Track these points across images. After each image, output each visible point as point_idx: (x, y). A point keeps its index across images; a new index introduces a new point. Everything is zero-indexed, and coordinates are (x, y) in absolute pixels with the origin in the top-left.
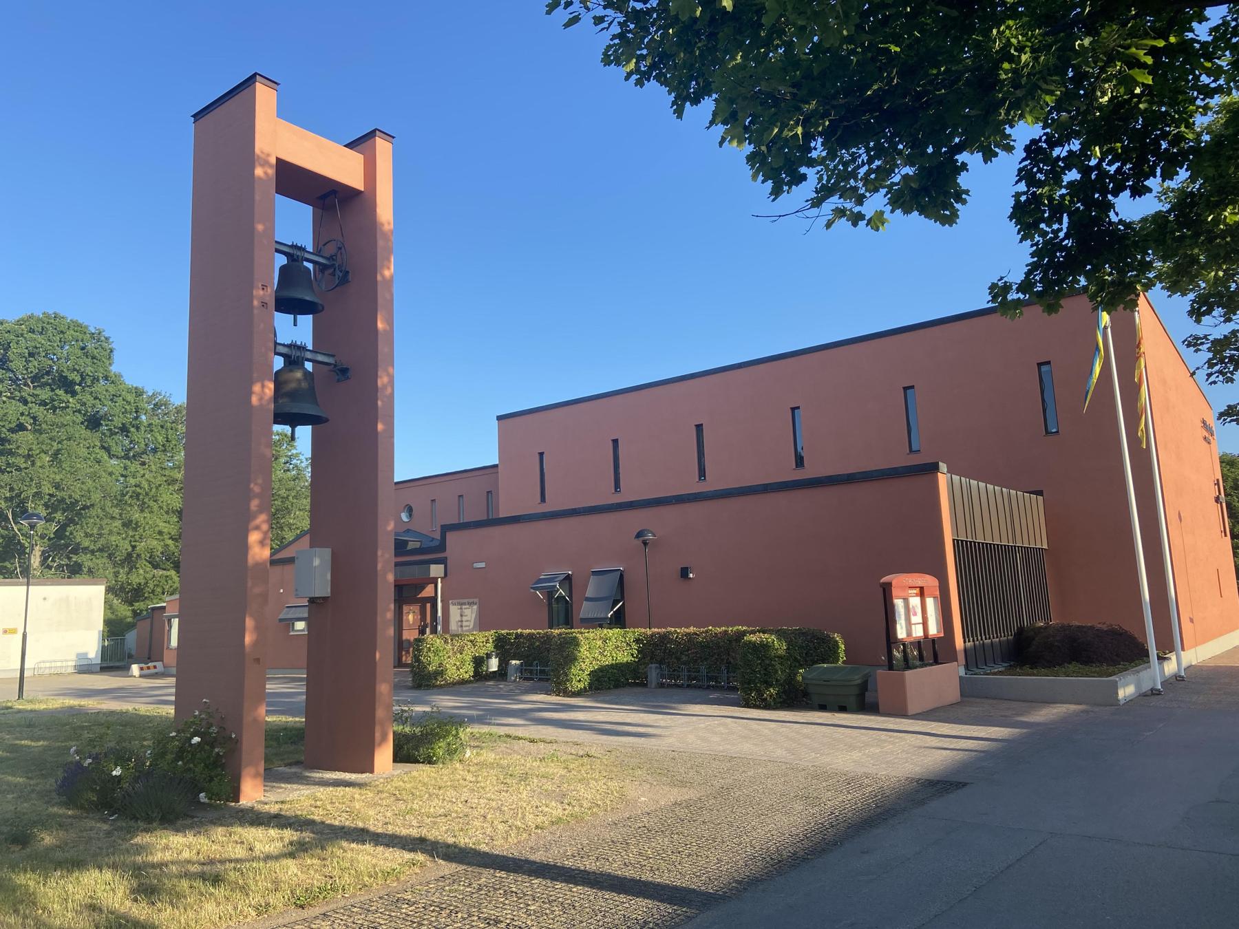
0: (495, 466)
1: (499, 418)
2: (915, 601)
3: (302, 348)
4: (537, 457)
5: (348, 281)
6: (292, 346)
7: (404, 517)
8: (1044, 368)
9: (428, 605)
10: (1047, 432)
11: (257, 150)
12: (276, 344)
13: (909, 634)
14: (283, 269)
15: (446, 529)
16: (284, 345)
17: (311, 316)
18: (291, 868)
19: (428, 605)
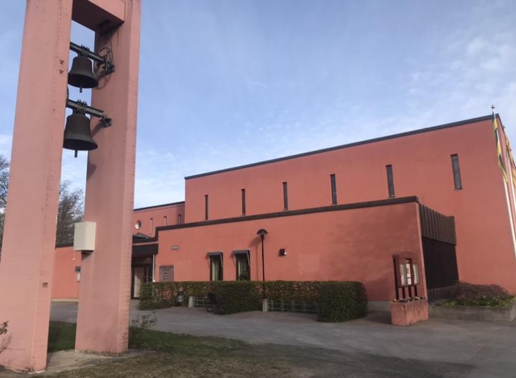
0: (184, 202)
1: (186, 178)
2: (408, 266)
3: (84, 105)
4: (204, 198)
5: (112, 72)
6: (79, 103)
7: (137, 226)
8: (454, 158)
9: (148, 268)
10: (456, 188)
11: (88, 223)
12: (68, 100)
13: (407, 282)
14: (75, 60)
15: (158, 229)
16: (74, 102)
17: (90, 90)
18: (154, 356)
19: (148, 268)
